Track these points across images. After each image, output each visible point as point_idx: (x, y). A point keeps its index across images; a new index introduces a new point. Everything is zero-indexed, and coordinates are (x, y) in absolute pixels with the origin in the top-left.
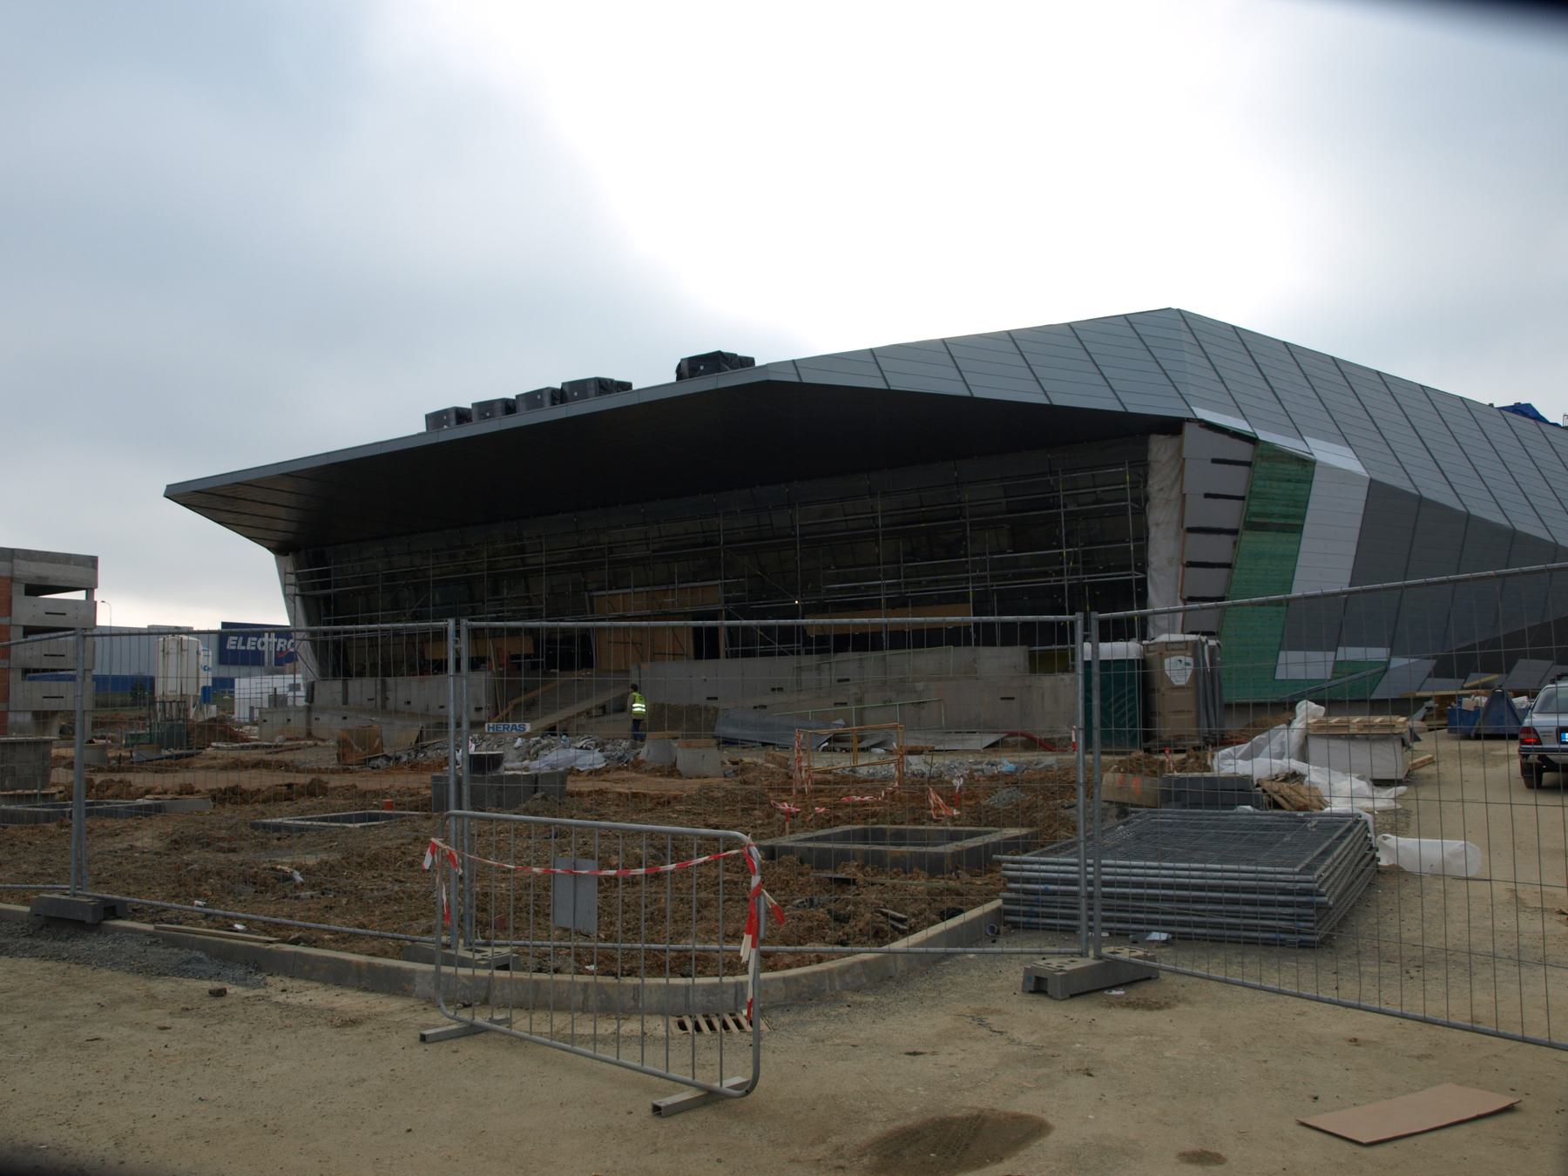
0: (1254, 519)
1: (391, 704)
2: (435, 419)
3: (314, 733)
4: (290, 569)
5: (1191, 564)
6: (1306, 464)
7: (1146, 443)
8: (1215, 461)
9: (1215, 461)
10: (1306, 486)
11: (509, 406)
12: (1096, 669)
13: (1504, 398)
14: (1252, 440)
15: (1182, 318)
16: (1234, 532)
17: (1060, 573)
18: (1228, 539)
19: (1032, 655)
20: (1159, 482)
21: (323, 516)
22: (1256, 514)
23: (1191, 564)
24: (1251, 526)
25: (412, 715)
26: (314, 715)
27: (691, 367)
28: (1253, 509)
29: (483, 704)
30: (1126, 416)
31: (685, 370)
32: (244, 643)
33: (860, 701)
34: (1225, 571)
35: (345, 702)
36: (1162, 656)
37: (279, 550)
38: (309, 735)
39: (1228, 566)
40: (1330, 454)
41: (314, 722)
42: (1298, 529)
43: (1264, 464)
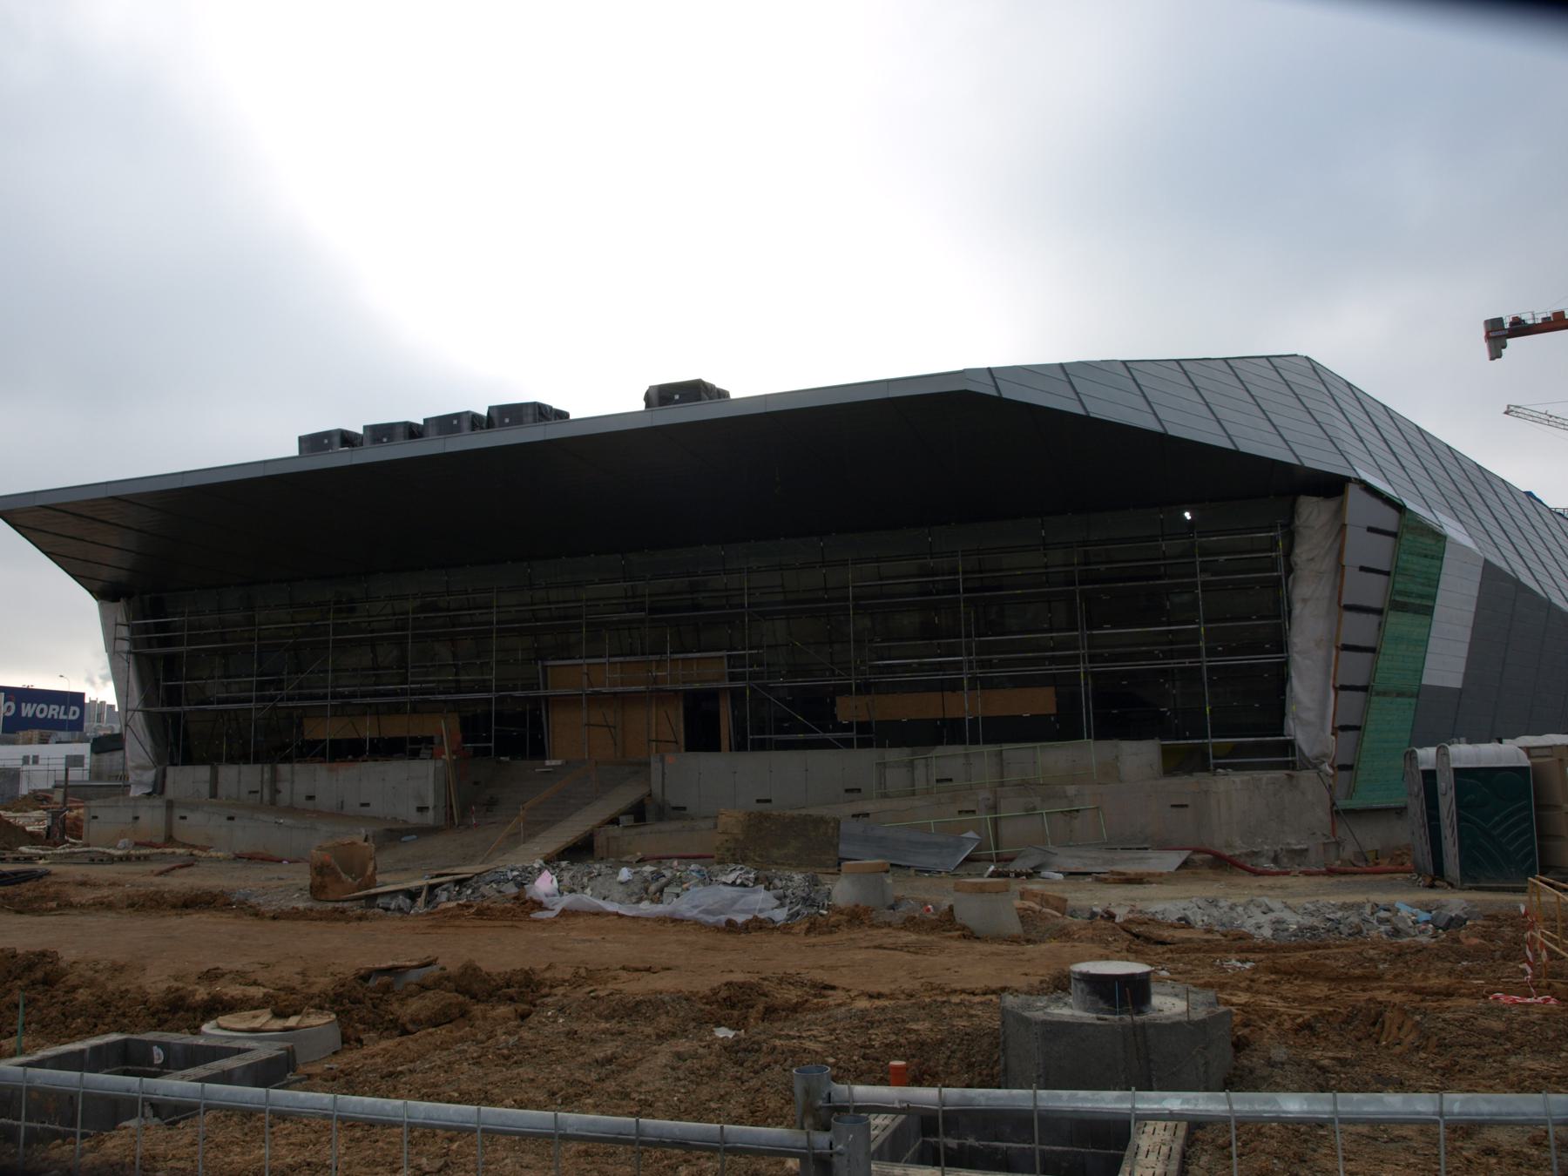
0: (1398, 598)
1: (284, 798)
2: (312, 443)
3: (177, 836)
4: (121, 619)
5: (1346, 648)
6: (1440, 537)
7: (1294, 501)
8: (1370, 529)
9: (1370, 529)
10: (1437, 563)
11: (412, 431)
12: (1445, 784)
13: (1523, 486)
14: (1400, 508)
15: (1314, 367)
16: (1379, 612)
17: (1075, 659)
19: (1166, 752)
20: (1311, 551)
21: (165, 553)
22: (1400, 593)
23: (1346, 648)
25: (320, 814)
26: (178, 812)
27: (661, 396)
29: (430, 802)
31: (654, 398)
32: (66, 713)
33: (994, 808)
34: (1369, 655)
35: (214, 795)
37: (104, 593)
38: (170, 840)
39: (1372, 650)
40: (1453, 530)
41: (176, 821)
42: (1428, 611)
43: (1410, 537)
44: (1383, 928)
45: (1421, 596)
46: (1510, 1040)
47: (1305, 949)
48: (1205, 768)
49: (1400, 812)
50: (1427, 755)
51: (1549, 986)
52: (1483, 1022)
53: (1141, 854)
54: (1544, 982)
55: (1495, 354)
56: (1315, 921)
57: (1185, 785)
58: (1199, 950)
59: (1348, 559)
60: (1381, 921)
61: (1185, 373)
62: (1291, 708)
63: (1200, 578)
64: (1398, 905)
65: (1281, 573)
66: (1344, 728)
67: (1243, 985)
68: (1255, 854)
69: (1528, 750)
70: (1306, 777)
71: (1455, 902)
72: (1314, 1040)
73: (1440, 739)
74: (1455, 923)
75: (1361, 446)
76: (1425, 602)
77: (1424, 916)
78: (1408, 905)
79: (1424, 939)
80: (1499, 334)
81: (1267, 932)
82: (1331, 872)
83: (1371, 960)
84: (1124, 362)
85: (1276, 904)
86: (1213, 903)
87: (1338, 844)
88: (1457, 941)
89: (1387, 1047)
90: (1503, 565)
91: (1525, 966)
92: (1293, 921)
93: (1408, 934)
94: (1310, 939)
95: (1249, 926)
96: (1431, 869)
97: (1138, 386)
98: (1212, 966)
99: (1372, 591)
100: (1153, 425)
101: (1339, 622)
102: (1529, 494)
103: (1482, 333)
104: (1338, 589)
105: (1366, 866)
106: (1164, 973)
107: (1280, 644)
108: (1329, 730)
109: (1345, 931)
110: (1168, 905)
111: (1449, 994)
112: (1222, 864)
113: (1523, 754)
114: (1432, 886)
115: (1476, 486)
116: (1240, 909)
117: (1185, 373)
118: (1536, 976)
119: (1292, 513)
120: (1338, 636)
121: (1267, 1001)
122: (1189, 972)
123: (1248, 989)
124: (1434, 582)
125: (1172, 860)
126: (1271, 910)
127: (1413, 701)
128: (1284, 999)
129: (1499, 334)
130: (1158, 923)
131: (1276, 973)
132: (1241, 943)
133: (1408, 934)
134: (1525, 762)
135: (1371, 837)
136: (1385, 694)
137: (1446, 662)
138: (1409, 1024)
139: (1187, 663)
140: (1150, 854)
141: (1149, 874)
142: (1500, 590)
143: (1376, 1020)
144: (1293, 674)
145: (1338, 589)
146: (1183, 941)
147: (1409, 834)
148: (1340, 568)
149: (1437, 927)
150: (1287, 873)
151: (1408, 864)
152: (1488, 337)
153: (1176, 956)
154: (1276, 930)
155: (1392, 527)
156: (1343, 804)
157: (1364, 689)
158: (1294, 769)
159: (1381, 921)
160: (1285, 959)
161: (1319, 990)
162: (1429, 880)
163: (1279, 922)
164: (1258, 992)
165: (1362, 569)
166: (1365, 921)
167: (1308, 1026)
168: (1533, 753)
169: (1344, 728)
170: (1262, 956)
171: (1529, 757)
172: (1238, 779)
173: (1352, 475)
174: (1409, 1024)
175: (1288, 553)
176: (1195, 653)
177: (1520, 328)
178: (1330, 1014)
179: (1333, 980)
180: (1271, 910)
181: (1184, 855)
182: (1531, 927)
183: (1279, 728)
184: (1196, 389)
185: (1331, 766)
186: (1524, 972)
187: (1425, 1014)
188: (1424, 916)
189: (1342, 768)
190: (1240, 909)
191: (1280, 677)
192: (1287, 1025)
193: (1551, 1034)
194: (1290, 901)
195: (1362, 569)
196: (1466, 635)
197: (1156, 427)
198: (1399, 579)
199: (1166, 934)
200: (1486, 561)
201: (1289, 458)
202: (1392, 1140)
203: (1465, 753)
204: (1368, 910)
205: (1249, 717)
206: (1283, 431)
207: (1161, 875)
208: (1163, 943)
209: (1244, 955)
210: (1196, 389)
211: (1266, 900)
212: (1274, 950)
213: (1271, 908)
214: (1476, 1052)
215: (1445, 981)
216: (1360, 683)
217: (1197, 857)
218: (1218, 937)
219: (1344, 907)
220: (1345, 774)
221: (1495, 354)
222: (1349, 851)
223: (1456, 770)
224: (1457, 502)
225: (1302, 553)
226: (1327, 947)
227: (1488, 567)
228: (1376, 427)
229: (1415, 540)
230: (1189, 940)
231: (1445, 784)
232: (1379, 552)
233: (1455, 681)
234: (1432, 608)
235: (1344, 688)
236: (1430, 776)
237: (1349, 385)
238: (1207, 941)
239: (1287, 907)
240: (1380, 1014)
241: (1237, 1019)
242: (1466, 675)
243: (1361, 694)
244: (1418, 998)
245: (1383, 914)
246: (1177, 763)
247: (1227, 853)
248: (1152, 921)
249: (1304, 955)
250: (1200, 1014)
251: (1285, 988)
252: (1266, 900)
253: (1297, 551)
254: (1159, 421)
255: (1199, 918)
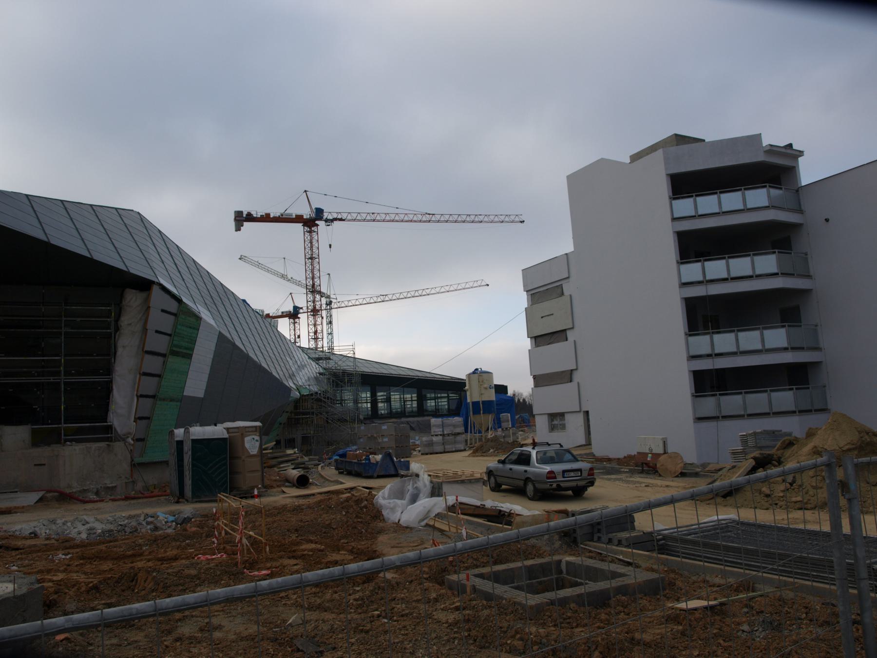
5: (145, 374)
6: (198, 318)
8: (163, 311)
9: (163, 311)
12: (187, 447)
13: (242, 296)
14: (179, 301)
16: (164, 355)
18: (161, 359)
19: (34, 433)
20: (130, 320)
23: (145, 374)
24: (174, 353)
28: (175, 342)
30: (128, 273)
34: (156, 379)
36: (243, 436)
39: (159, 376)
40: (205, 315)
42: (189, 356)
44: (149, 527)
45: (186, 349)
46: (199, 579)
47: (104, 543)
48: (58, 442)
49: (166, 463)
50: (179, 432)
51: (224, 548)
52: (187, 572)
53: (12, 495)
54: (222, 547)
55: (238, 229)
56: (112, 527)
57: (43, 453)
58: (39, 551)
59: (149, 326)
60: (148, 523)
61: (66, 209)
62: (112, 407)
63: (63, 330)
64: (159, 514)
65: (112, 330)
66: (141, 418)
67: (62, 569)
68: (85, 490)
69: (228, 429)
70: (118, 446)
71: (187, 509)
72: (98, 595)
73: (185, 423)
74: (187, 520)
75: (162, 265)
76: (188, 352)
77: (171, 518)
78: (164, 513)
79: (169, 531)
80: (241, 219)
81: (84, 536)
82: (127, 498)
83: (140, 545)
84: (27, 196)
85: (91, 519)
86: (53, 521)
87: (133, 482)
88: (186, 530)
89: (138, 593)
90: (228, 335)
91: (214, 540)
92: (99, 527)
93: (162, 529)
94: (109, 537)
95: (73, 534)
96: (178, 493)
97: (34, 211)
98: (46, 559)
99: (160, 344)
100: (42, 237)
101: (142, 360)
102: (244, 301)
103: (233, 217)
104: (143, 341)
105: (148, 494)
106: (15, 568)
107: (109, 371)
108: (133, 419)
109: (128, 530)
110: (24, 526)
111: (175, 558)
112: (65, 498)
113: (225, 431)
114: (178, 502)
115: (220, 295)
116: (69, 524)
117: (66, 209)
118: (219, 544)
119: (122, 296)
120: (141, 367)
121: (74, 576)
122: (31, 565)
123: (65, 571)
124: (193, 341)
125: (34, 497)
126: (88, 523)
127: (179, 404)
128: (85, 573)
129: (241, 219)
130: (15, 537)
131: (83, 559)
132: (66, 543)
133: (162, 529)
134: (226, 436)
135: (152, 477)
136: (164, 400)
137: (196, 385)
138: (150, 578)
139: (52, 379)
140: (19, 494)
141: (15, 508)
142: (226, 349)
143: (134, 578)
144: (114, 387)
145: (143, 341)
146: (30, 547)
147: (169, 475)
148: (145, 330)
149: (177, 524)
150: (102, 501)
151: (168, 491)
152: (235, 220)
153: (24, 556)
154: (89, 534)
155: (174, 311)
156: (138, 460)
157: (153, 397)
158: (111, 441)
159: (148, 523)
160: (87, 552)
161: (106, 566)
162: (176, 499)
163: (91, 529)
164: (70, 572)
165: (157, 332)
166: (140, 524)
167: (96, 588)
168: (231, 431)
169: (141, 418)
170: (78, 550)
171: (228, 433)
172: (78, 448)
173: (156, 280)
174: (150, 578)
175: (117, 319)
176: (58, 373)
177: (250, 218)
178: (109, 579)
179: (116, 559)
180: (88, 523)
181: (41, 494)
182: (218, 519)
183: (105, 419)
184: (71, 219)
185: (133, 439)
186: (214, 543)
187: (159, 571)
188: (171, 518)
189: (138, 440)
190: (69, 524)
191: (107, 389)
192: (83, 589)
193: (219, 573)
194: (99, 517)
195: (157, 332)
196: (207, 370)
197: (44, 238)
198: (175, 338)
199: (19, 543)
200: (220, 332)
201: (121, 266)
202: (129, 644)
203: (199, 431)
204: (142, 518)
205: (85, 412)
206: (86, 242)
207: (23, 507)
208: (17, 549)
209: (67, 551)
210: (71, 219)
211: (85, 517)
212: (85, 546)
213: (84, 523)
214: (181, 588)
215: (175, 552)
216: (151, 394)
217: (49, 495)
218: (53, 541)
219: (130, 517)
220: (139, 443)
221: (238, 229)
222: (139, 486)
223: (193, 440)
224: (209, 301)
225: (125, 320)
226: (116, 541)
227: (221, 335)
228: (172, 256)
229: (185, 318)
230: (35, 545)
231: (187, 447)
232: (166, 323)
233: (201, 394)
234: (191, 355)
235: (142, 396)
236: (180, 443)
237: (160, 232)
238: (46, 545)
239: (97, 520)
240: (136, 575)
241: (52, 590)
242: (206, 391)
243: (151, 400)
244: (160, 563)
245: (150, 519)
246: (39, 440)
247: (68, 491)
248: (14, 537)
249: (103, 547)
250: (24, 590)
251: (88, 568)
252: (85, 517)
253: (122, 319)
254: (46, 234)
255: (43, 531)
